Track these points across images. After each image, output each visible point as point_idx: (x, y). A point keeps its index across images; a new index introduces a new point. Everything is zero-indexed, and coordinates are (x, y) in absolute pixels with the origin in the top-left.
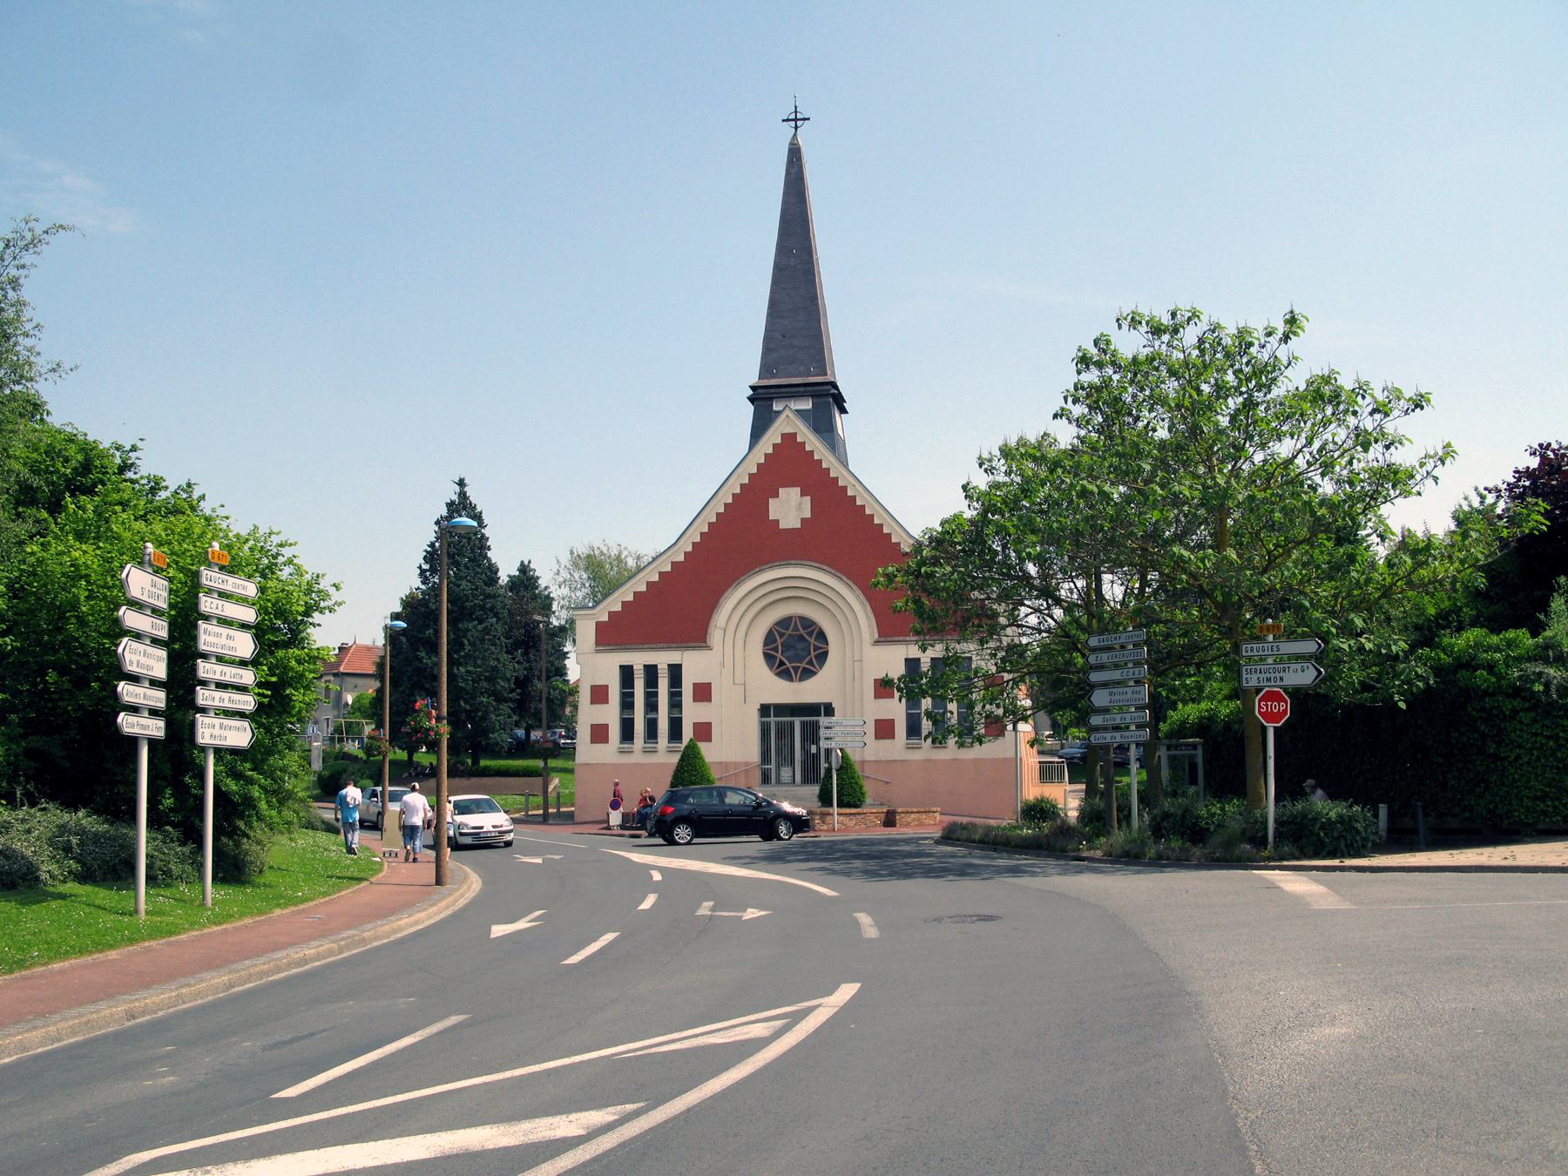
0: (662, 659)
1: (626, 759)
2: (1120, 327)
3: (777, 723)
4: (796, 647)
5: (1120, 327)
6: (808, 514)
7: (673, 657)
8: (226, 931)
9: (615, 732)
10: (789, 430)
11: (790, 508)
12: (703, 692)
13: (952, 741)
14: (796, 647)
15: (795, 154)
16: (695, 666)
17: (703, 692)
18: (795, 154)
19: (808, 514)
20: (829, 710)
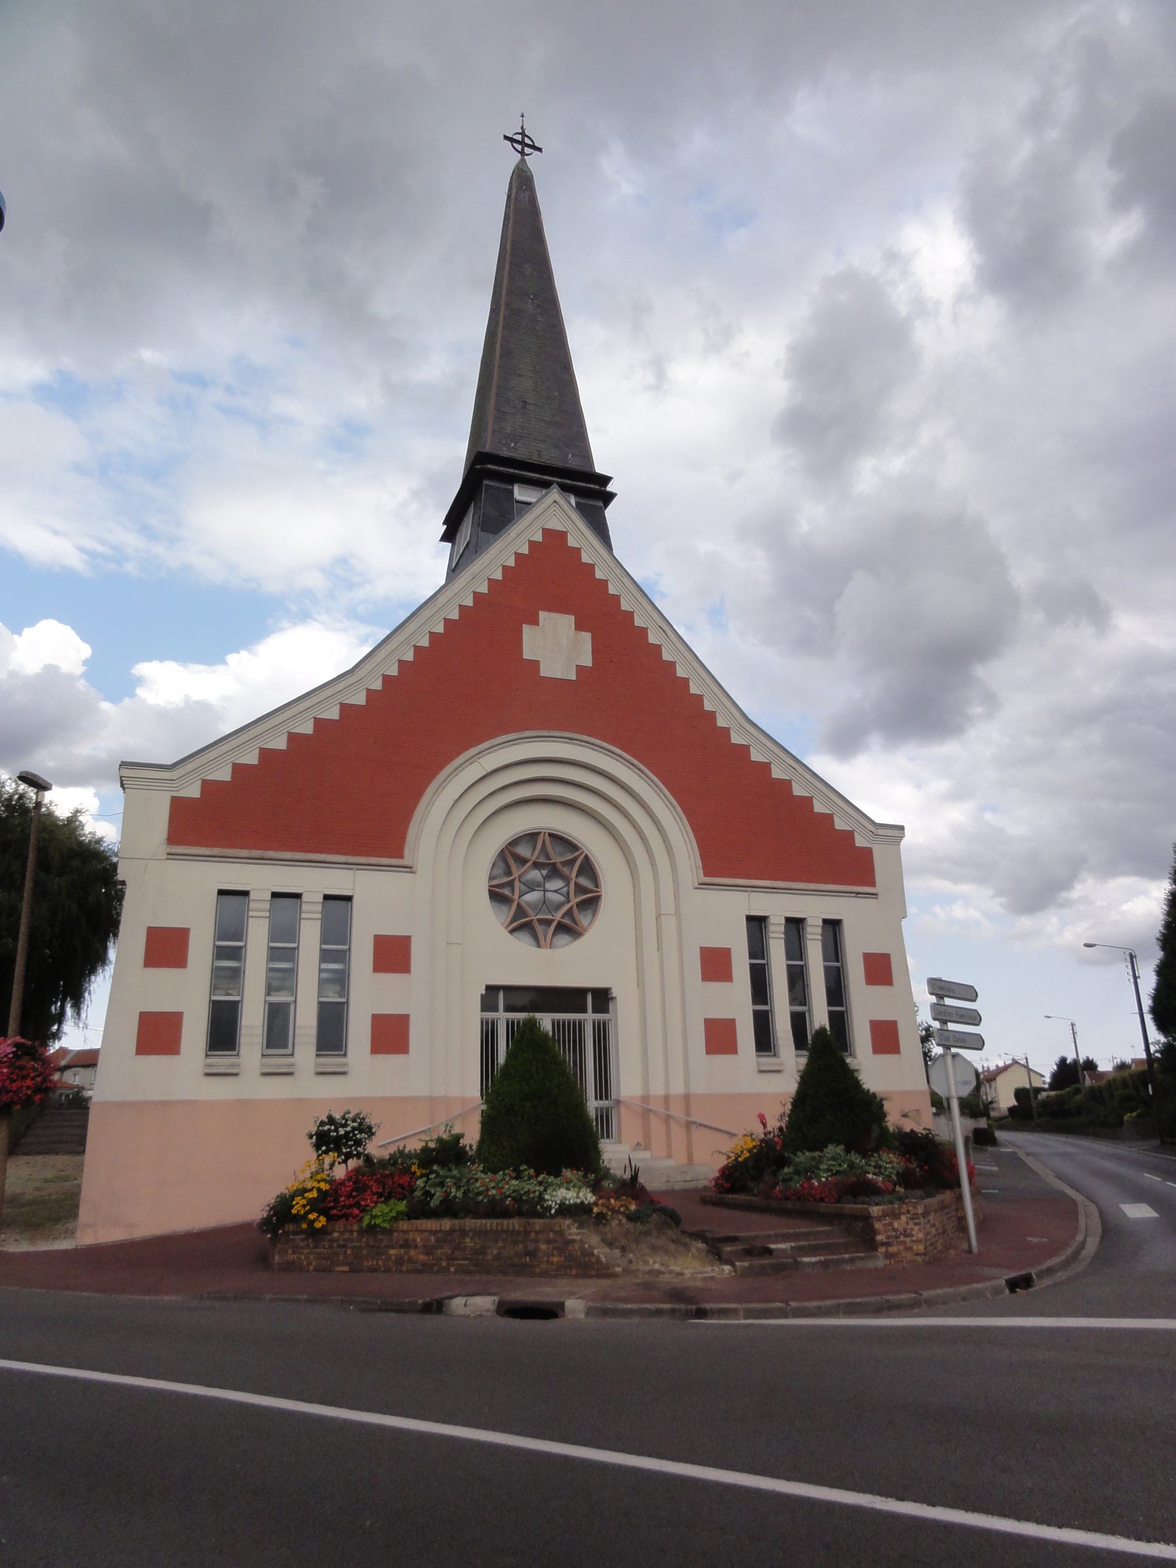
0: (313, 880)
1: (277, 1089)
2: (26, 778)
3: (510, 1025)
4: (547, 884)
5: (26, 778)
6: (587, 661)
7: (337, 880)
8: (852, 1296)
9: (195, 1031)
10: (555, 525)
11: (556, 646)
12: (393, 954)
13: (934, 999)
14: (547, 884)
15: (522, 183)
16: (380, 898)
17: (393, 954)
18: (522, 183)
19: (587, 661)
20: (603, 998)
